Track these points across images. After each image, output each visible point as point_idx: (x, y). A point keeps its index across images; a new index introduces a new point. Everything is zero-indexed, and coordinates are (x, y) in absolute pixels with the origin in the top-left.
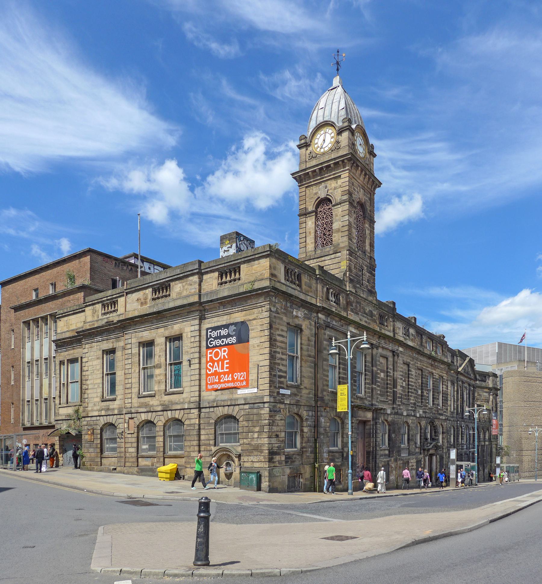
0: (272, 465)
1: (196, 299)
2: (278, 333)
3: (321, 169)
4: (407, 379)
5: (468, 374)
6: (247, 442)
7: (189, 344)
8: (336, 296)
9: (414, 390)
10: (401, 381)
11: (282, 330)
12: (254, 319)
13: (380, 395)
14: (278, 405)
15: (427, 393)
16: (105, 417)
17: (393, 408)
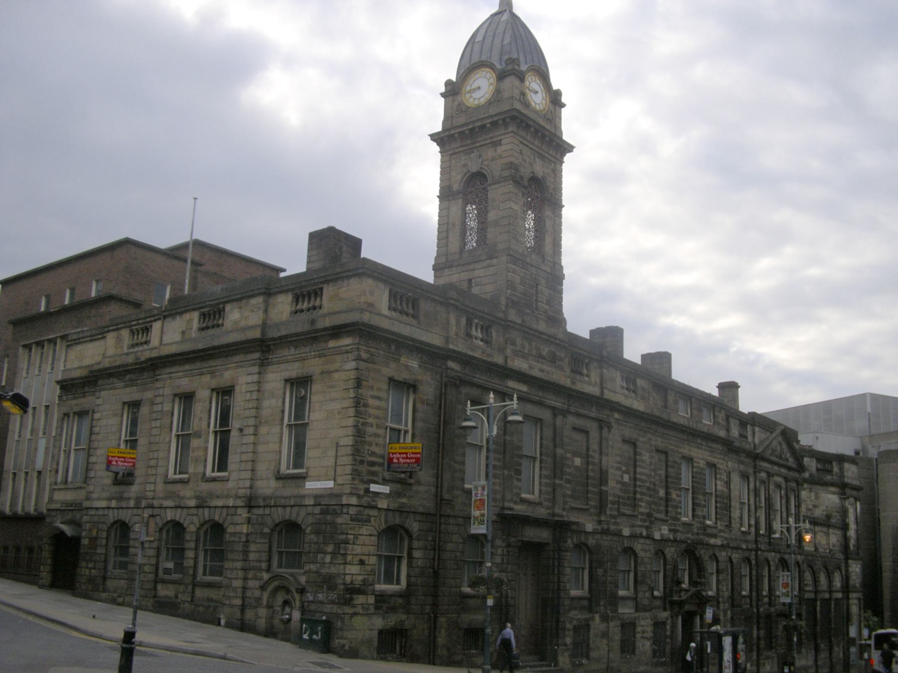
1: (257, 334)
2: (371, 393)
3: (471, 130)
4: (632, 470)
5: (781, 458)
6: (315, 569)
7: (242, 404)
8: (486, 329)
9: (648, 489)
10: (619, 473)
11: (379, 389)
12: (337, 371)
13: (571, 496)
14: (367, 511)
15: (678, 496)
16: (116, 511)
17: (600, 522)
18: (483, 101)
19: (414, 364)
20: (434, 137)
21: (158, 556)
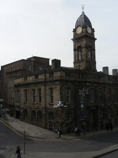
0: (62, 127)
18: (80, 33)
19: (70, 84)
20: (72, 39)
21: (32, 116)
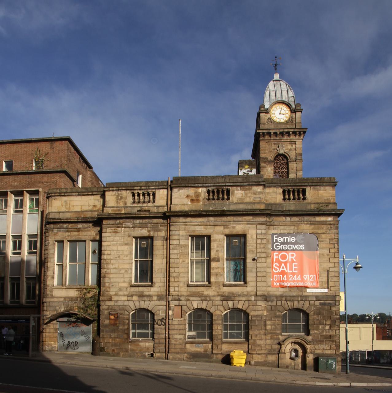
6: (319, 333)
12: (323, 233)
